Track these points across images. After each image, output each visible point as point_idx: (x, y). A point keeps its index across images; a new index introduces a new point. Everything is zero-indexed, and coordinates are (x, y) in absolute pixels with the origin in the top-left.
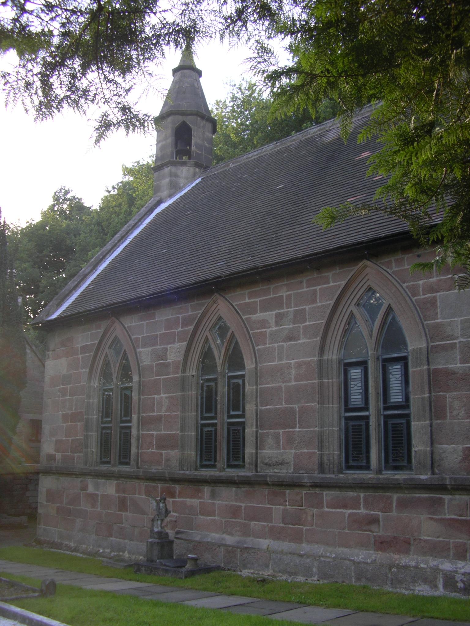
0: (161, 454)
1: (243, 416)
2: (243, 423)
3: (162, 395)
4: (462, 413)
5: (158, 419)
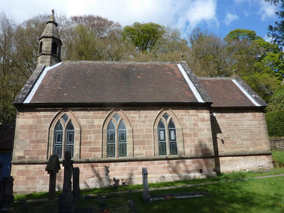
0: (92, 154)
1: (126, 142)
2: (126, 144)
3: (91, 135)
4: (190, 142)
5: (90, 143)
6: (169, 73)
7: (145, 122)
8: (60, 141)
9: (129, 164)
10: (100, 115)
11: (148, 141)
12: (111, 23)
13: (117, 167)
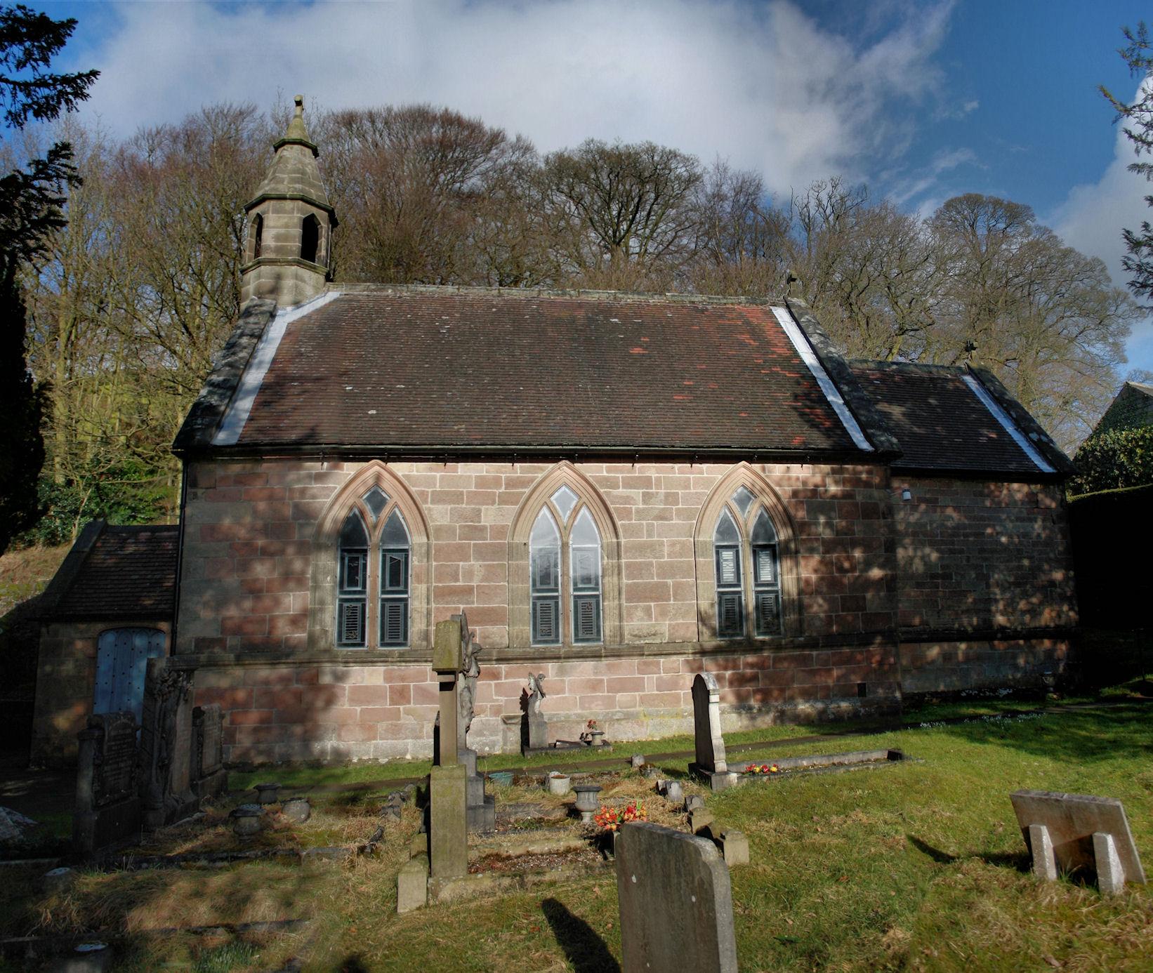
5: (469, 590)
6: (745, 338)
7: (666, 519)
8: (357, 585)
9: (609, 667)
10: (503, 490)
11: (677, 586)
12: (496, 138)
13: (567, 679)
